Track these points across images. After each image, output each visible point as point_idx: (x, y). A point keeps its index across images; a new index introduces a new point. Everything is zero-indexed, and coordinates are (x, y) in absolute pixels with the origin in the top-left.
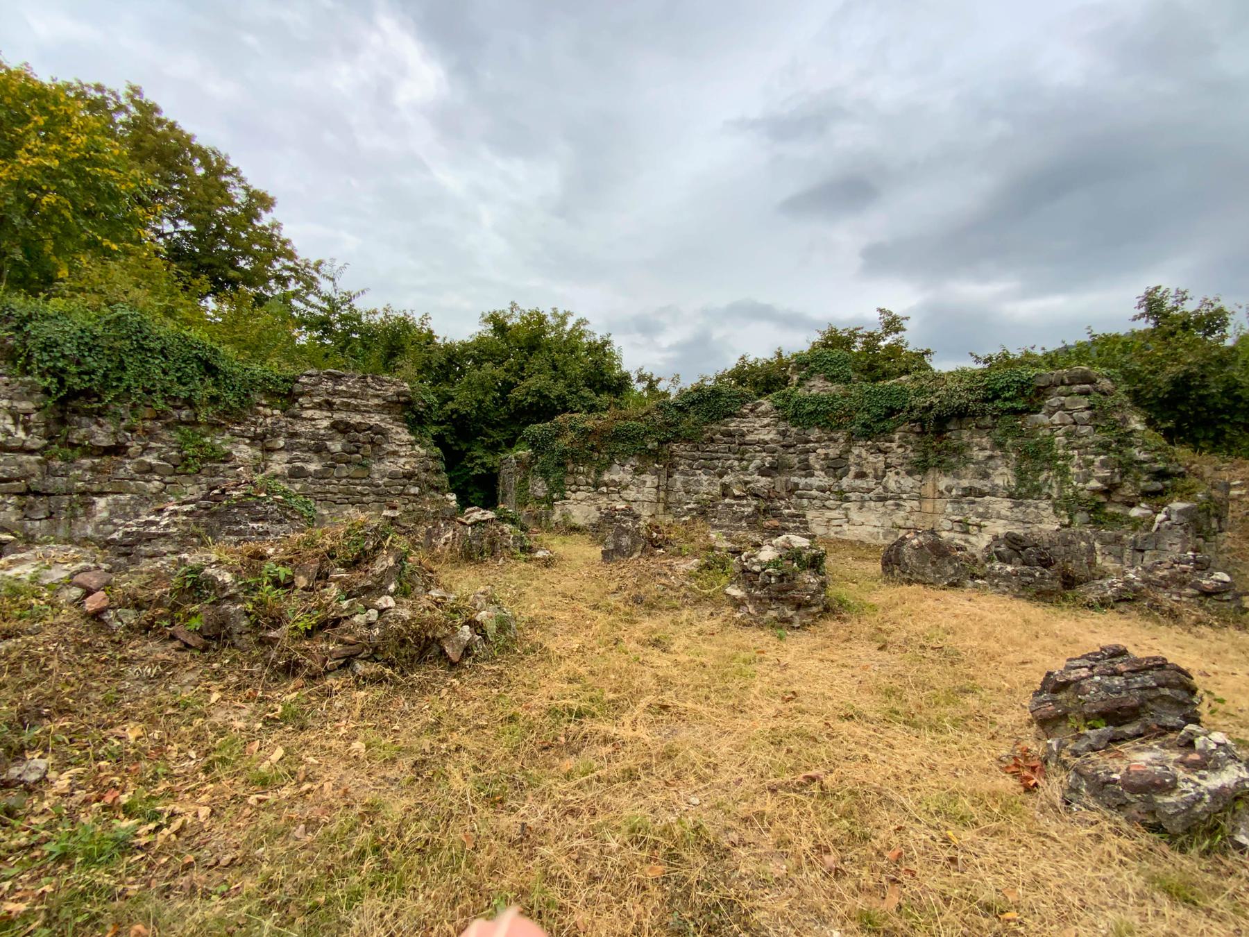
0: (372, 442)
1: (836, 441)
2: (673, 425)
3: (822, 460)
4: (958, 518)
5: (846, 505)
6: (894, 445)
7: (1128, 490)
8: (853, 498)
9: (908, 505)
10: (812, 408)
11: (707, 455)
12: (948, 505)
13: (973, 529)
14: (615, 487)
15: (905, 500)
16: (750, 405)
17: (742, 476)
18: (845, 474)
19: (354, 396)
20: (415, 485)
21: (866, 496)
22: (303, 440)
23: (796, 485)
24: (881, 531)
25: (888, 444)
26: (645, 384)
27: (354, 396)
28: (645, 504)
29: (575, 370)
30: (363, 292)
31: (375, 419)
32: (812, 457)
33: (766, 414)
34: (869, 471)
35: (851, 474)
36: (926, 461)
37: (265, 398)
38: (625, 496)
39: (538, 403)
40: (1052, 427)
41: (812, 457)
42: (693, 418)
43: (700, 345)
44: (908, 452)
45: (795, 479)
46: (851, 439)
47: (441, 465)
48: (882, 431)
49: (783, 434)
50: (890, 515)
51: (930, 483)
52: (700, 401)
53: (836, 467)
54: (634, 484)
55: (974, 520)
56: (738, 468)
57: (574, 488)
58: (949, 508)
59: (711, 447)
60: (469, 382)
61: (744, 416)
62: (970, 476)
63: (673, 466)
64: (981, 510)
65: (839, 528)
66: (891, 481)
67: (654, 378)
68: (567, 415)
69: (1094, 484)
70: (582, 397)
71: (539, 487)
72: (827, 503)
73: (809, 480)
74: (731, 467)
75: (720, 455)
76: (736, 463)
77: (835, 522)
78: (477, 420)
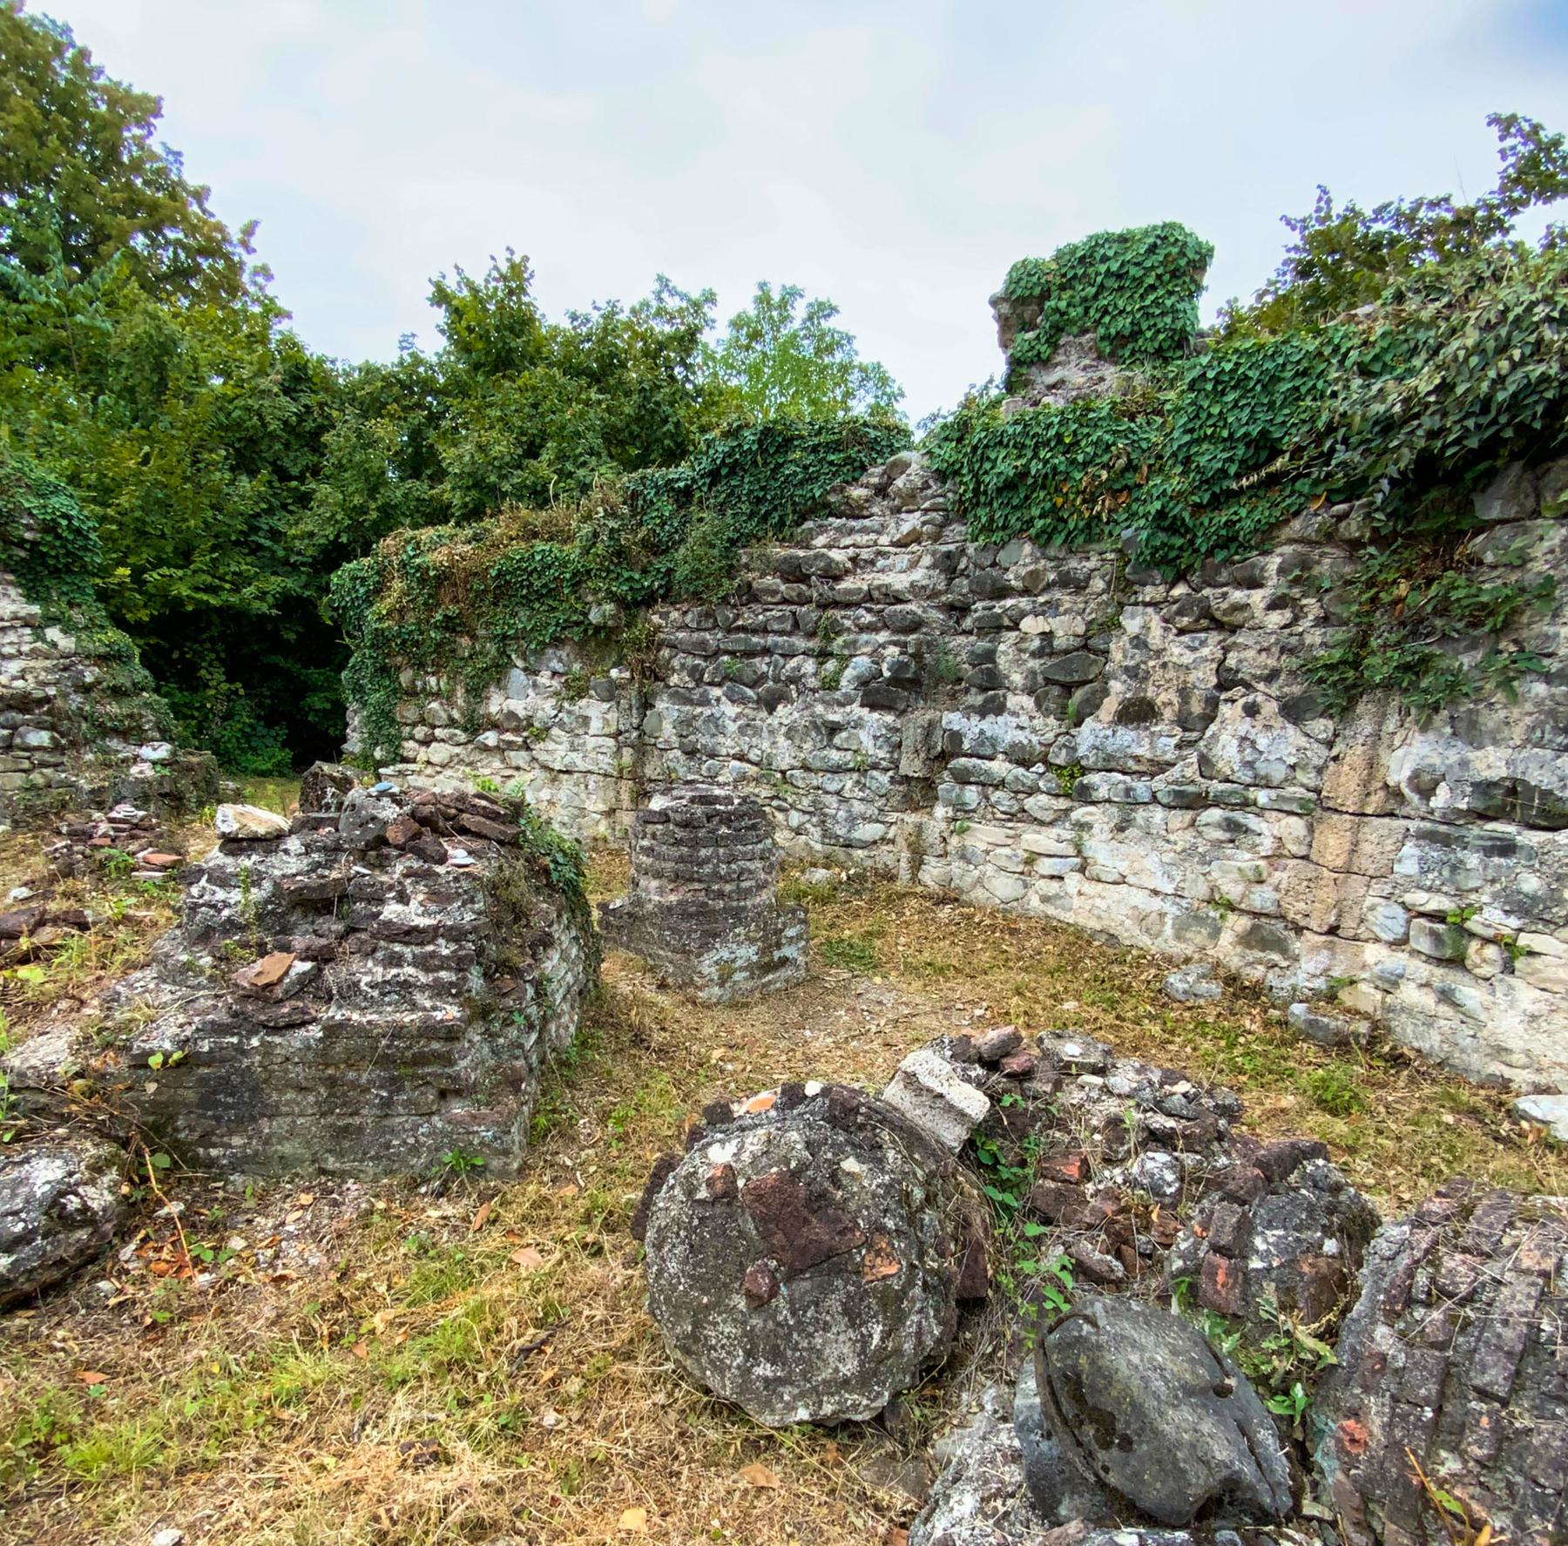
1: (1078, 585)
3: (1034, 655)
4: (1435, 903)
5: (1081, 813)
6: (1258, 598)
8: (1102, 793)
9: (1270, 829)
10: (1006, 467)
11: (738, 641)
12: (1409, 849)
13: (1485, 958)
14: (517, 731)
15: (1261, 812)
16: (874, 475)
17: (819, 709)
18: (1091, 707)
20: (40, 726)
21: (1141, 787)
23: (956, 737)
24: (1172, 910)
25: (1238, 595)
28: (592, 778)
33: (909, 501)
34: (1166, 697)
35: (1110, 706)
36: (1356, 664)
38: (543, 757)
44: (1305, 624)
45: (953, 720)
46: (1124, 588)
48: (1224, 543)
49: (948, 565)
50: (1204, 861)
51: (1354, 754)
52: (734, 468)
54: (561, 725)
55: (1492, 918)
56: (812, 682)
57: (420, 732)
58: (1409, 860)
59: (748, 618)
62: (1518, 734)
63: (654, 674)
64: (1531, 883)
65: (1054, 886)
72: (1029, 803)
74: (795, 679)
75: (771, 639)
76: (809, 666)
77: (1045, 866)
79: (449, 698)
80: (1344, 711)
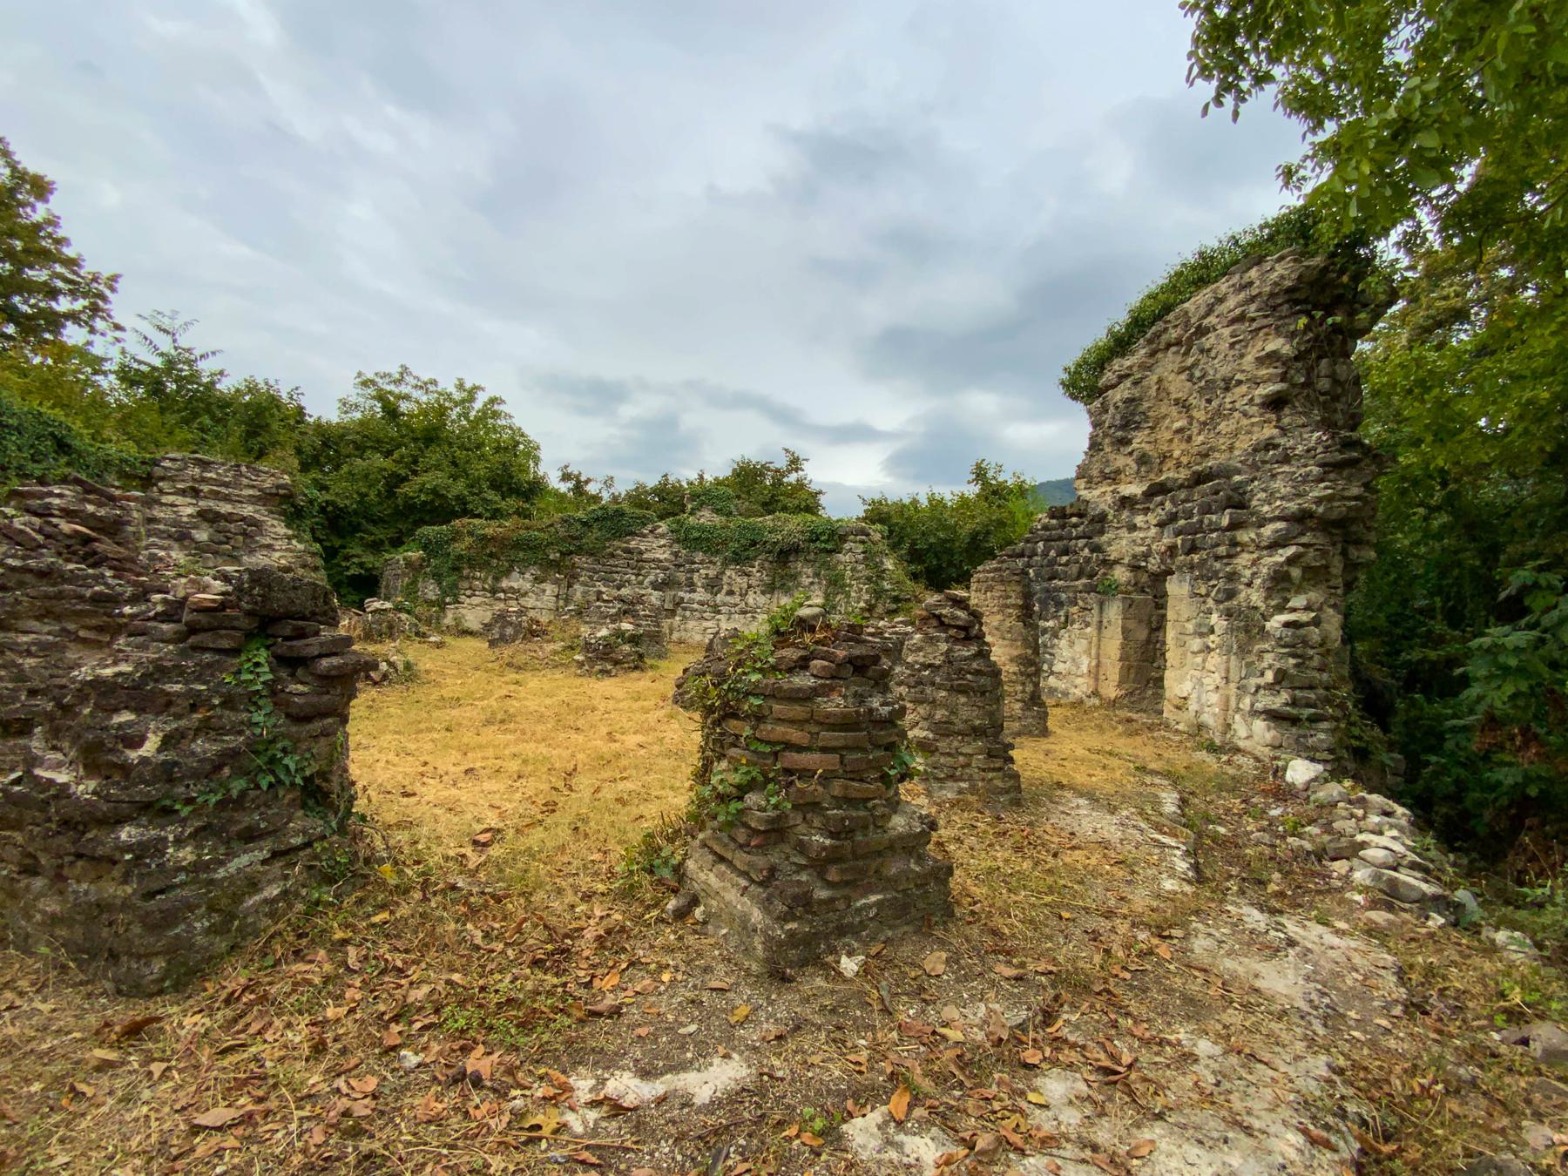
0: (245, 534)
2: (576, 538)
7: (880, 610)
10: (696, 535)
16: (650, 527)
18: (719, 591)
19: (227, 485)
22: (161, 527)
26: (570, 485)
27: (227, 485)
29: (480, 469)
30: (214, 353)
31: (247, 510)
32: (696, 576)
33: (662, 536)
34: (736, 589)
37: (119, 479)
39: (432, 501)
40: (845, 564)
41: (696, 576)
42: (596, 533)
43: (663, 431)
45: (681, 594)
46: (725, 564)
47: (320, 562)
49: (676, 554)
53: (713, 585)
59: (611, 562)
60: (350, 473)
61: (644, 536)
63: (575, 577)
66: (750, 598)
67: (583, 478)
68: (466, 520)
69: (862, 604)
70: (484, 500)
71: (431, 591)
73: (692, 595)
78: (355, 512)
79: (484, 581)
80: (772, 592)
